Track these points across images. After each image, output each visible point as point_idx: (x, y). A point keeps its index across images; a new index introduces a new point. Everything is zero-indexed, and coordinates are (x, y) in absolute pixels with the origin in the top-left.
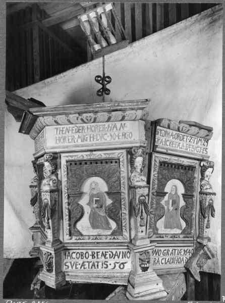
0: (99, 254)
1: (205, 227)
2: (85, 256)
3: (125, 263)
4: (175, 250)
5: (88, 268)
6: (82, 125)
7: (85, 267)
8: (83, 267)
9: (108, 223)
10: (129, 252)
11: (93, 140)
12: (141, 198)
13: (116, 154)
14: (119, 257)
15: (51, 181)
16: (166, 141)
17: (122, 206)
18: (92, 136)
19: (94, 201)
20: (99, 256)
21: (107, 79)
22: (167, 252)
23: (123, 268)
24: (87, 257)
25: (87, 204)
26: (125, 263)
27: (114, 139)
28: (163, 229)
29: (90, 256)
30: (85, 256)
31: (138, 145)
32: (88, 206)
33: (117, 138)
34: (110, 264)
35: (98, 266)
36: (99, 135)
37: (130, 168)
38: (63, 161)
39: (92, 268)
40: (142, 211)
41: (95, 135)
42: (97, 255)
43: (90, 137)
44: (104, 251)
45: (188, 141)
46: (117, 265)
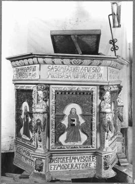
1: (105, 139)
2: (84, 165)
13: (90, 88)
15: (44, 106)
17: (54, 124)
21: (113, 49)
30: (84, 165)
38: (53, 89)
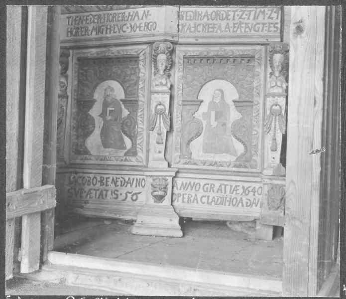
0: (108, 180)
3: (139, 193)
4: (225, 186)
5: (94, 198)
6: (97, 13)
7: (92, 195)
8: (89, 196)
9: (122, 140)
10: (144, 179)
11: (110, 33)
12: (159, 107)
14: (131, 186)
16: (196, 27)
18: (109, 27)
19: (108, 112)
20: (109, 183)
22: (211, 188)
23: (136, 200)
24: (94, 183)
25: (100, 116)
26: (139, 193)
27: (135, 31)
28: (201, 153)
29: (98, 183)
31: (162, 38)
32: (101, 119)
33: (138, 29)
34: (121, 194)
35: (106, 195)
36: (117, 25)
37: (153, 70)
39: (99, 198)
40: (275, 127)
41: (112, 25)
42: (107, 181)
43: (107, 29)
44: (115, 177)
45: (237, 18)
46: (129, 196)
